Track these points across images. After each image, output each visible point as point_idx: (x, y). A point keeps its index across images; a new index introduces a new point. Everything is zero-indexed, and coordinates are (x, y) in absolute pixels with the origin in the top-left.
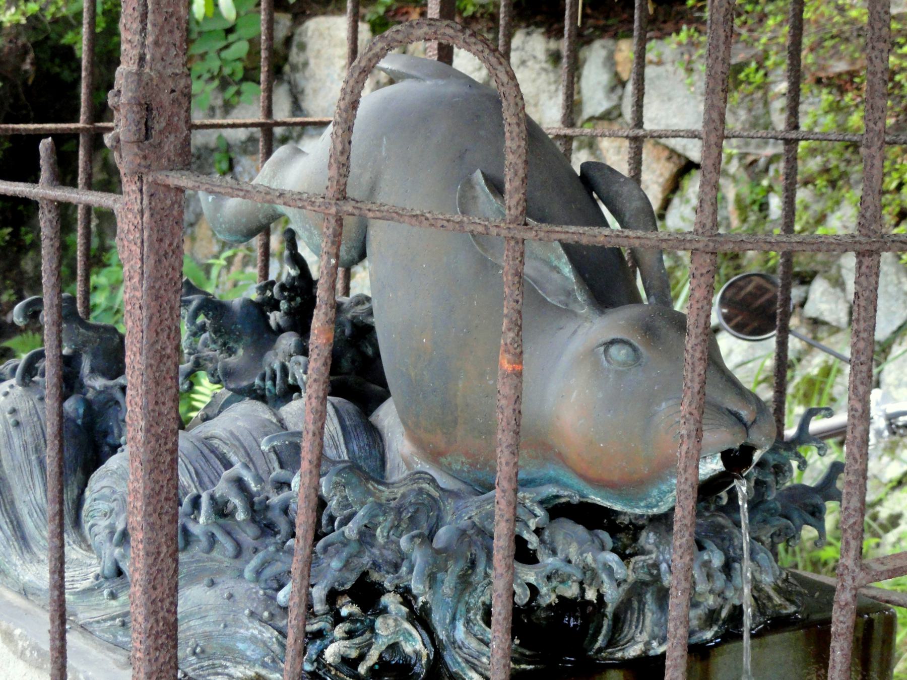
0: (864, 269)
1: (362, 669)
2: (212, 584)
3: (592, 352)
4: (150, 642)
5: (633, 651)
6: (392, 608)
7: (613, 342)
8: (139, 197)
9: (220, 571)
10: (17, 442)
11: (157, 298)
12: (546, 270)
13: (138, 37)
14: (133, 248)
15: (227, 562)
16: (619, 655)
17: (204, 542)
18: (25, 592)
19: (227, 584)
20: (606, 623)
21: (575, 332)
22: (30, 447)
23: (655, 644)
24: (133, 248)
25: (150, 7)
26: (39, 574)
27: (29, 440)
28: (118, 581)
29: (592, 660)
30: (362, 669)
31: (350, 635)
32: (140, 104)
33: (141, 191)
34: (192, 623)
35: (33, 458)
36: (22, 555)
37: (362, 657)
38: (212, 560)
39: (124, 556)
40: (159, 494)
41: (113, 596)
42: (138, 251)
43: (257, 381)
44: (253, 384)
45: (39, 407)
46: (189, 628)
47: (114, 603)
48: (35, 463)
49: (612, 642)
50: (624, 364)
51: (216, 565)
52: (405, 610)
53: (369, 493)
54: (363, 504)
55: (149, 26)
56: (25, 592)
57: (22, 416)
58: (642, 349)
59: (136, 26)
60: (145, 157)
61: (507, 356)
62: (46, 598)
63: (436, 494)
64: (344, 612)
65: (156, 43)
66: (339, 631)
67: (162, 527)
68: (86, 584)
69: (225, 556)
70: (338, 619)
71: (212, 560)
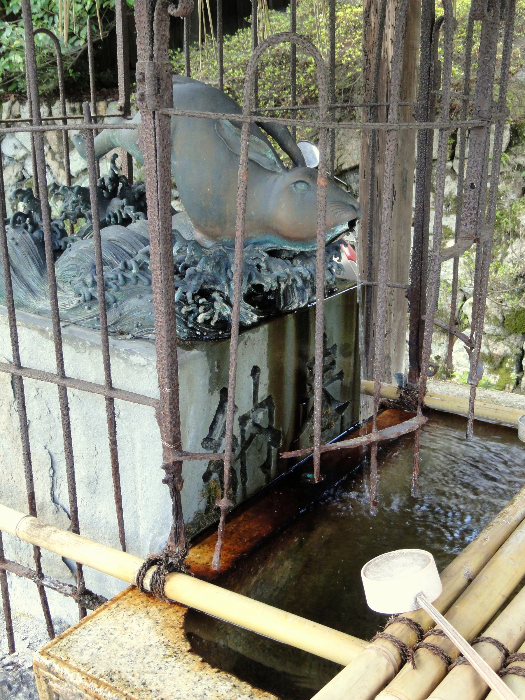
0: (443, 136)
1: (213, 323)
2: (141, 297)
3: (288, 187)
4: (167, 317)
5: (295, 307)
6: (217, 298)
7: (297, 182)
8: (153, 121)
9: (142, 292)
10: (18, 251)
11: (163, 166)
12: (260, 156)
13: (148, 47)
14: (150, 145)
15: (145, 288)
16: (290, 309)
17: (133, 280)
18: (39, 313)
19: (148, 297)
20: (282, 297)
21: (275, 181)
22: (26, 253)
23: (301, 303)
24: (150, 145)
25: (155, 32)
26: (45, 304)
27: (25, 250)
28: (92, 302)
29: (281, 311)
30: (213, 323)
31: (205, 310)
32: (155, 77)
33: (154, 118)
34: (134, 314)
35: (28, 257)
36: (34, 298)
37: (211, 319)
38: (138, 287)
39: (94, 291)
40: (167, 253)
41: (90, 308)
42: (153, 146)
43: (107, 219)
44: (105, 220)
45: (23, 236)
46: (133, 316)
47: (89, 311)
48: (30, 259)
49: (285, 304)
50: (304, 190)
51: (139, 289)
52: (221, 298)
53: (203, 253)
54: (201, 257)
55: (155, 41)
56: (39, 313)
57: (17, 240)
58: (311, 184)
59: (148, 41)
60: (158, 102)
61: (322, 179)
62: (50, 314)
63: (225, 251)
64: (200, 301)
65: (159, 49)
66: (201, 309)
67: (169, 268)
68: (72, 306)
69: (143, 285)
70: (199, 305)
71: (138, 287)
